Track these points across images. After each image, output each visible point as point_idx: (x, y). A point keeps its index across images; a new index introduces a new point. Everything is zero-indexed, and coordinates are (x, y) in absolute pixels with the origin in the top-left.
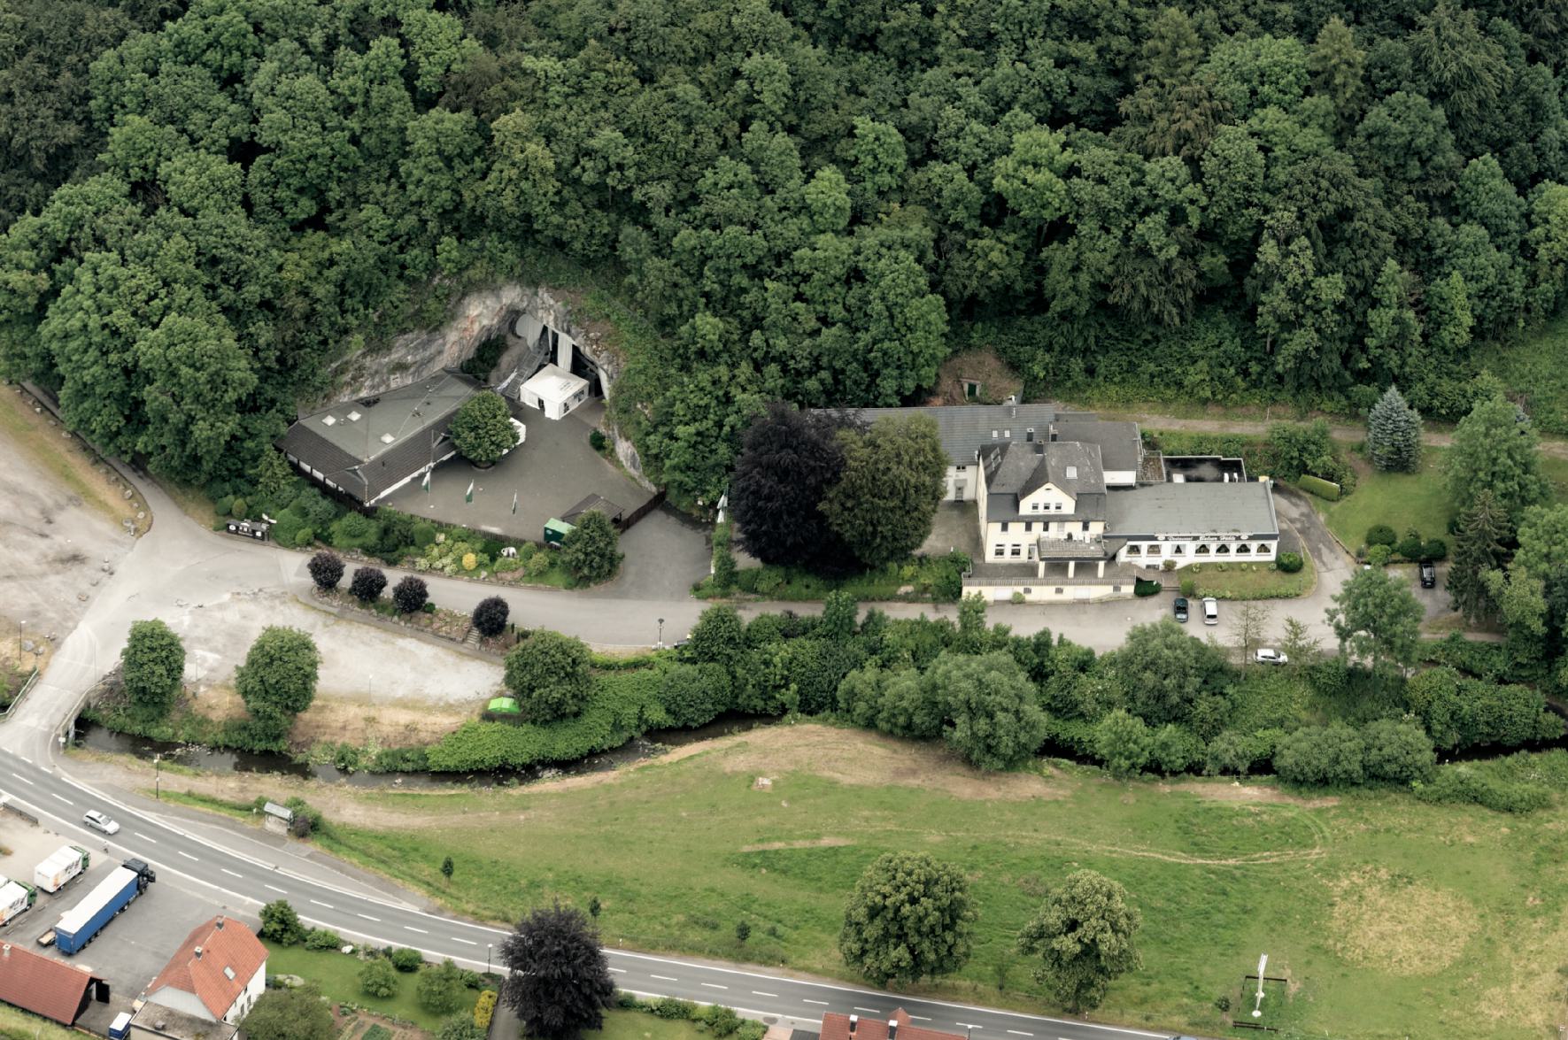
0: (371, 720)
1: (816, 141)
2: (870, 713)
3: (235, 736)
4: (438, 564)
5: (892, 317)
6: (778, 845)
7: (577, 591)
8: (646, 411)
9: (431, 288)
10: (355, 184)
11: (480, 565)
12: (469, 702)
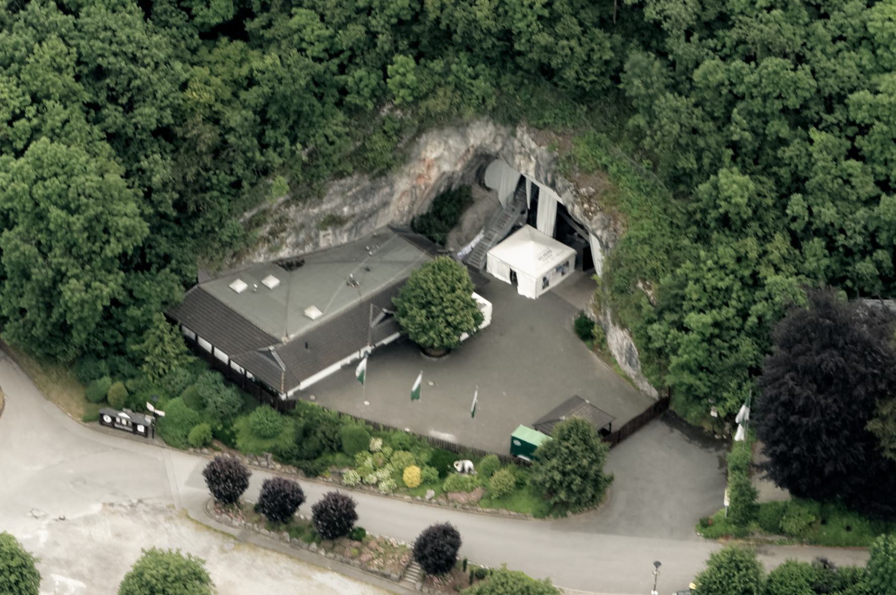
4: (372, 478)
7: (549, 521)
8: (649, 293)
9: (378, 121)
11: (426, 482)
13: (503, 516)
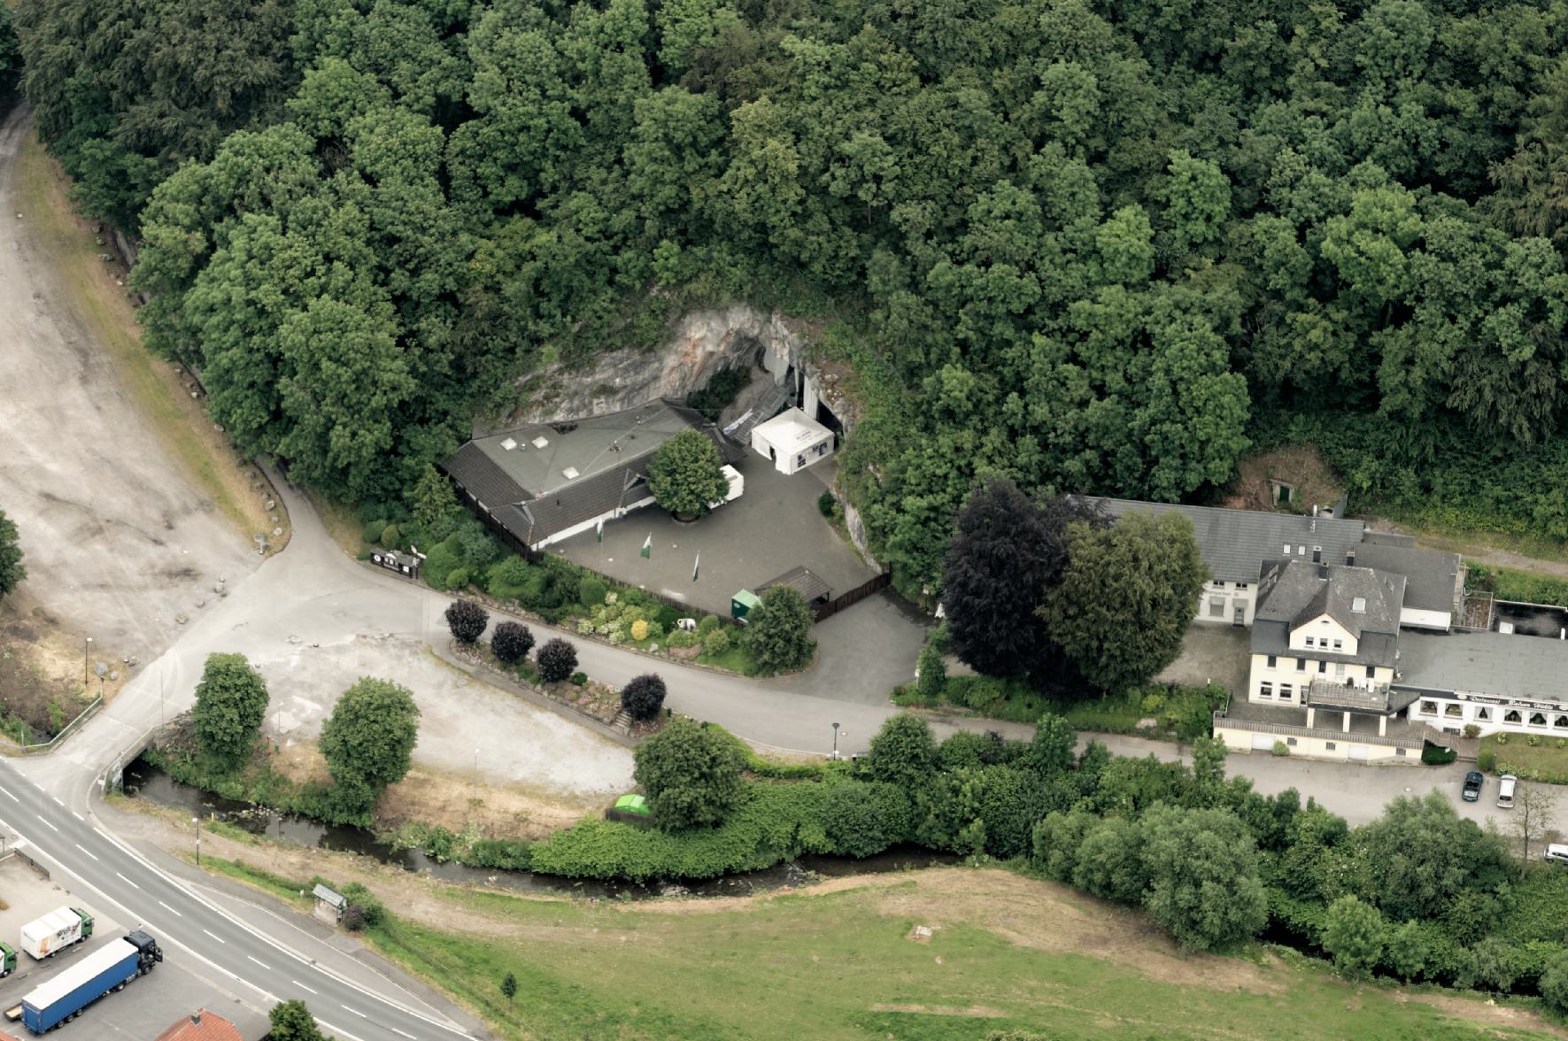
0: (476, 803)
1: (1125, 173)
2: (1065, 865)
3: (314, 803)
4: (604, 629)
5: (1175, 392)
6: (915, 1008)
7: (758, 680)
8: (878, 474)
9: (646, 299)
10: (574, 166)
11: (651, 636)
12: (597, 796)
13: (716, 672)
